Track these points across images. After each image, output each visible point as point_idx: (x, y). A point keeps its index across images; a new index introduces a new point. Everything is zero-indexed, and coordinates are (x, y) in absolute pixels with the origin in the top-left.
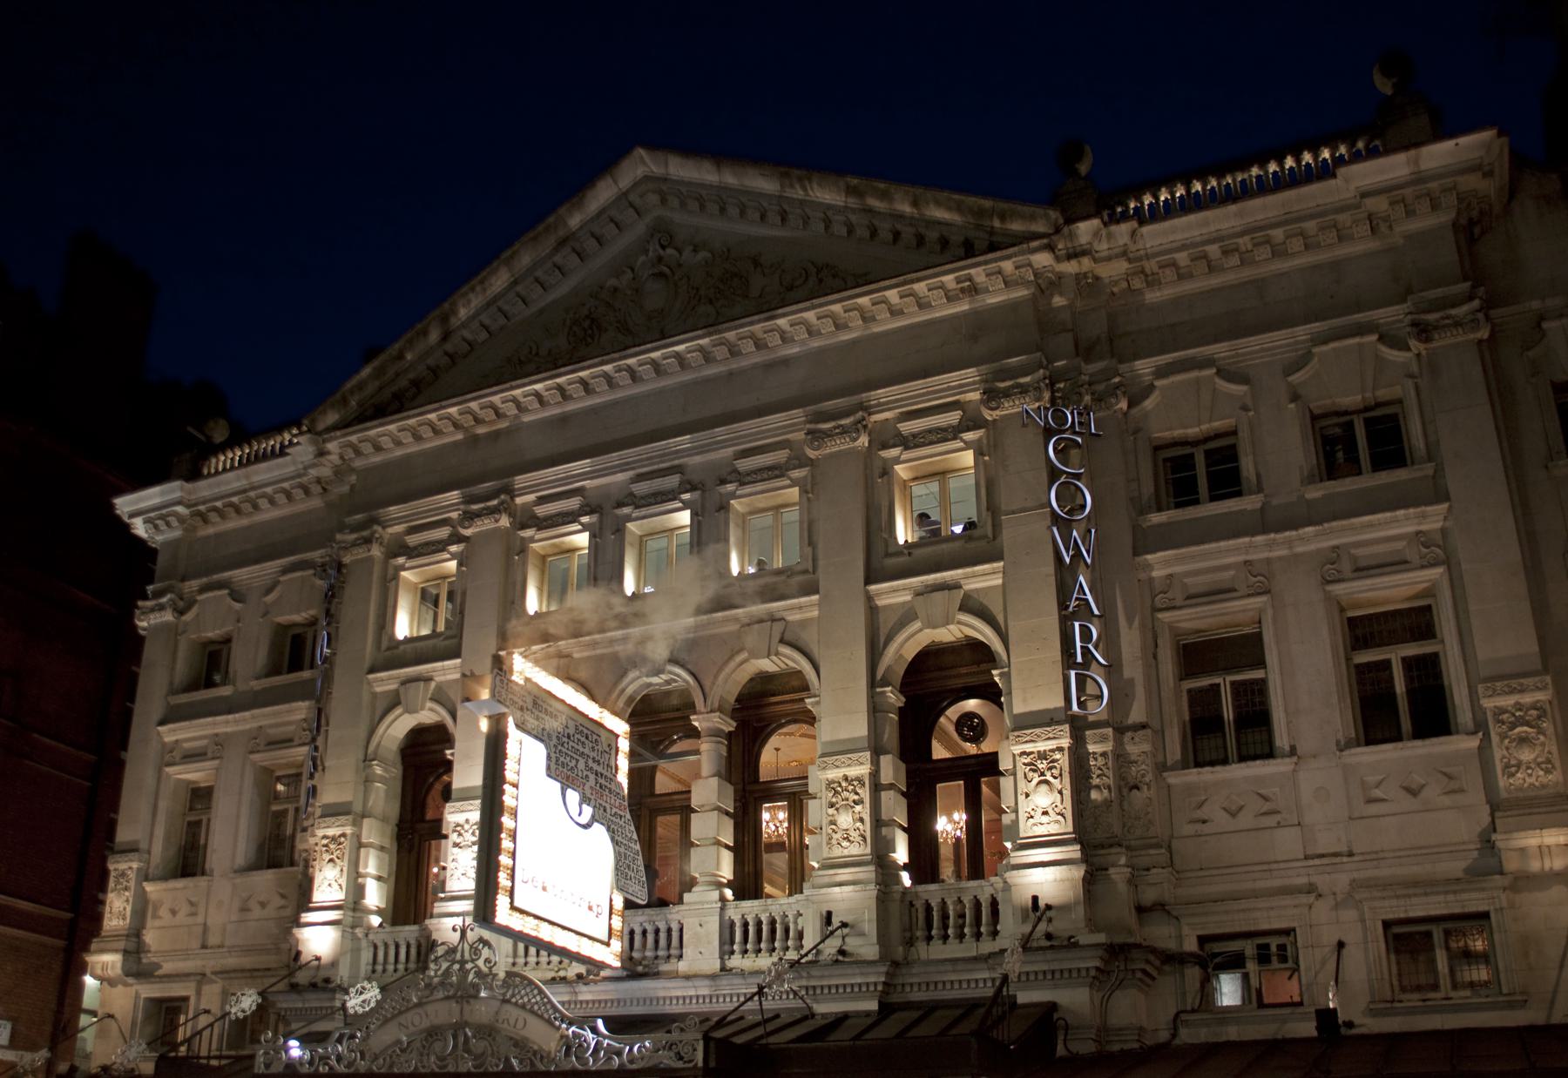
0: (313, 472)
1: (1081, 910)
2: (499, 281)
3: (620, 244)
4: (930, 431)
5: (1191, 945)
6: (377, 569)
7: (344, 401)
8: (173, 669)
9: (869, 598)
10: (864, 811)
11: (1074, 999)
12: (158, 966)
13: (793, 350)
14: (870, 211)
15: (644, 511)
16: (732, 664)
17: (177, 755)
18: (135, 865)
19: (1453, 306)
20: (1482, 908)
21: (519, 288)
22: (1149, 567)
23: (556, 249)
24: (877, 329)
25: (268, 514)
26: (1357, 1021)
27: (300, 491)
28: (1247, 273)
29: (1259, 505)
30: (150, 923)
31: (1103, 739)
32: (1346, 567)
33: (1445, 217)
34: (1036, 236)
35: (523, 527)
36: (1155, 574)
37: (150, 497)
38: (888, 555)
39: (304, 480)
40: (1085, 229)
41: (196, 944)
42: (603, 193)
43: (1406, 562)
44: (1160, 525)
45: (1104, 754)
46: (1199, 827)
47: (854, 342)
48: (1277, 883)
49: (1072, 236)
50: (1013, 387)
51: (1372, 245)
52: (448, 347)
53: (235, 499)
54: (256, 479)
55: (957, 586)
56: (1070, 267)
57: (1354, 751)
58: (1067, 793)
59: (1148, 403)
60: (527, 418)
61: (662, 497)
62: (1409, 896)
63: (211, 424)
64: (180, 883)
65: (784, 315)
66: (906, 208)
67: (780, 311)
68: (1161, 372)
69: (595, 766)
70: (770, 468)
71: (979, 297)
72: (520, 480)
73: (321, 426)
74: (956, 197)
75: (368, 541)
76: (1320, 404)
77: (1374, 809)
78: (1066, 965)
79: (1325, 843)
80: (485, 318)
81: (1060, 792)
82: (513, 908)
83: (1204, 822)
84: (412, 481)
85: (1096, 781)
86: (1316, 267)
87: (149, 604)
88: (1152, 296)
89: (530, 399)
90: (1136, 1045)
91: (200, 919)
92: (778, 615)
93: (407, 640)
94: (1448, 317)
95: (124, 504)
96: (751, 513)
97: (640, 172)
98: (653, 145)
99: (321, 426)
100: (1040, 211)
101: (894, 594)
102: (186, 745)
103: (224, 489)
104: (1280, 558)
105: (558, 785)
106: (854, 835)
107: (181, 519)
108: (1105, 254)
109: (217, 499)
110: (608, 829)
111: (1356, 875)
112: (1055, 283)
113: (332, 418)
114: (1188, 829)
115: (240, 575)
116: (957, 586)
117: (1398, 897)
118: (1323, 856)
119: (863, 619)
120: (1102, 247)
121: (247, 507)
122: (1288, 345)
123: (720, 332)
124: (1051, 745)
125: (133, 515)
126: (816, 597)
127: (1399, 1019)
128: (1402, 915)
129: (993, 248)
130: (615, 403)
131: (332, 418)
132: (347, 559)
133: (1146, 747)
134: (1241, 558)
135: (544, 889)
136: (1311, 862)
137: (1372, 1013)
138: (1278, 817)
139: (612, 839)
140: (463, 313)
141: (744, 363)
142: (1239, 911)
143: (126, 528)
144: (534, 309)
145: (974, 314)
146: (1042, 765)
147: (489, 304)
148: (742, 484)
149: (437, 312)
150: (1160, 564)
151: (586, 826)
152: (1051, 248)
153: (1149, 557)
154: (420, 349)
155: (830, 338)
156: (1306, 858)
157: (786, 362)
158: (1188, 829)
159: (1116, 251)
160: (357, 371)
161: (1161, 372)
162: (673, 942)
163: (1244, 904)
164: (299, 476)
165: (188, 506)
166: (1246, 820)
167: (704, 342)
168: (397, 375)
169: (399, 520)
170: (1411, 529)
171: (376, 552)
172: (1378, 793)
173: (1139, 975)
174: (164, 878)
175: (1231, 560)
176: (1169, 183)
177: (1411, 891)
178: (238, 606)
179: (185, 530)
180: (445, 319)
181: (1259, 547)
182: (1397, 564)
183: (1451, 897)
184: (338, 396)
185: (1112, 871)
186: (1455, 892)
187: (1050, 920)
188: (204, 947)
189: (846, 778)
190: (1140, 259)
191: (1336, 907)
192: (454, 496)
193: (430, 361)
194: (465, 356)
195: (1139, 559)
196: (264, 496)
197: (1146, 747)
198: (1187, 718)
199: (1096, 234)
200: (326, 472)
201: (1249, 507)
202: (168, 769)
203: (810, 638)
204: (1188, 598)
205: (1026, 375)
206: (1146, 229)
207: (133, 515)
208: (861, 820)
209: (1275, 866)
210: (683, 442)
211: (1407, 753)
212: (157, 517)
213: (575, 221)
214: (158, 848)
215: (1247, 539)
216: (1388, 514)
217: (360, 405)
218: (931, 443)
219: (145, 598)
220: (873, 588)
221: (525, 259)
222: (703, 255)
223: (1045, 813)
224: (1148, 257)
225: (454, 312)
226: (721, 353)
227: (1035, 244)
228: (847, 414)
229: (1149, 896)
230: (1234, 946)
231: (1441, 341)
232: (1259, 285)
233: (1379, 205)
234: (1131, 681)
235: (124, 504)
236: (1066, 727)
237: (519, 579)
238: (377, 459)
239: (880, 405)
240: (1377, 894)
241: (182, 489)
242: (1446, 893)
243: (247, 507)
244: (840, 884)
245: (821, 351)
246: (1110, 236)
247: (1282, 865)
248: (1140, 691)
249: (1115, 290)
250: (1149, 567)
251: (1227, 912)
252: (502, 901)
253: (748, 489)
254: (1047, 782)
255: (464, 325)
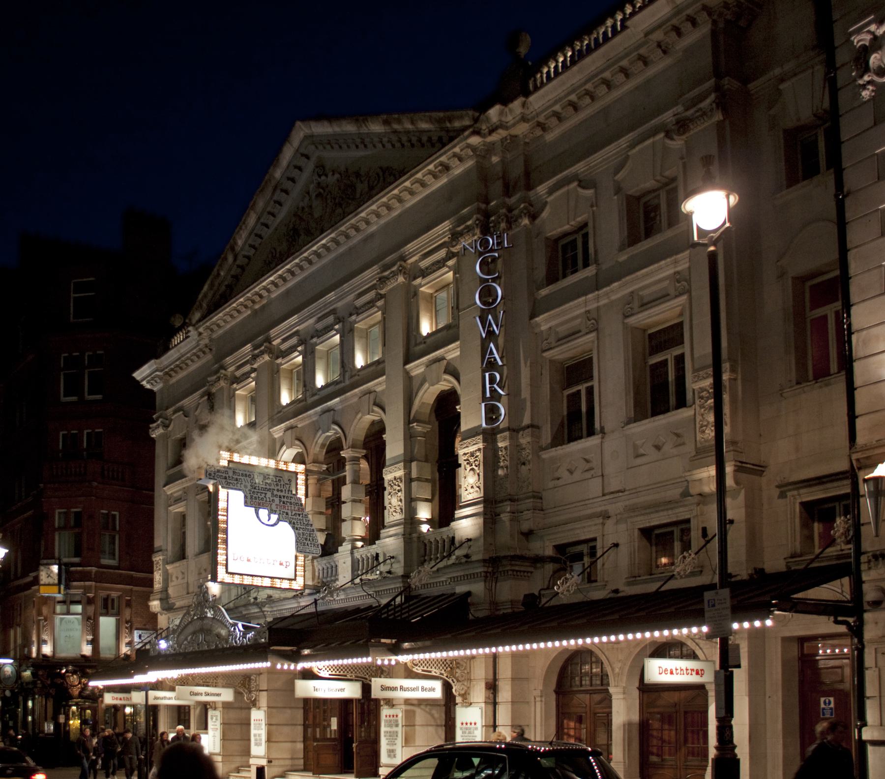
0: (202, 343)
1: (482, 540)
2: (252, 220)
3: (303, 178)
4: (433, 264)
5: (549, 552)
6: (226, 394)
7: (201, 306)
8: (167, 457)
9: (407, 373)
10: (401, 495)
11: (478, 588)
12: (174, 604)
13: (373, 228)
14: (395, 132)
15: (321, 339)
16: (356, 421)
17: (172, 500)
18: (161, 558)
19: (701, 102)
20: (687, 517)
21: (262, 220)
22: (538, 325)
23: (273, 194)
24: (408, 205)
25: (193, 367)
26: (621, 588)
27: (406, 193)
28: (598, 106)
29: (594, 272)
30: (171, 584)
31: (504, 439)
32: (636, 304)
33: (705, 29)
34: (465, 128)
35: (277, 358)
36: (543, 328)
37: (145, 371)
38: (416, 345)
39: (200, 347)
40: (494, 113)
41: (185, 592)
42: (287, 154)
43: (668, 295)
44: (546, 296)
45: (506, 448)
46: (556, 482)
47: (400, 216)
48: (589, 512)
49: (488, 119)
50: (464, 229)
51: (668, 61)
52: (238, 262)
53: (177, 363)
54: (182, 351)
55: (443, 358)
56: (494, 138)
57: (632, 425)
58: (482, 474)
59: (544, 215)
60: (273, 296)
61: (328, 329)
62: (649, 513)
63: (172, 319)
64: (177, 564)
65: (362, 211)
66: (409, 126)
67: (360, 209)
68: (551, 191)
69: (279, 493)
70: (368, 303)
71: (450, 172)
72: (273, 332)
73: (194, 321)
74: (427, 114)
75: (219, 379)
76: (633, 191)
77: (639, 461)
78: (471, 571)
79: (614, 484)
80: (250, 242)
81: (479, 475)
82: (227, 572)
83: (558, 479)
84: (223, 348)
85: (502, 464)
86: (637, 88)
87: (155, 425)
88: (550, 137)
89: (270, 286)
90: (510, 611)
91: (185, 581)
92: (372, 389)
93: (363, 368)
94: (697, 111)
95: (138, 375)
96: (370, 327)
97: (302, 135)
98: (303, 119)
99: (194, 321)
100: (464, 113)
101: (417, 368)
102: (175, 495)
103: (172, 359)
104: (604, 305)
105: (253, 509)
106: (398, 508)
107: (160, 378)
108: (512, 122)
109: (170, 365)
110: (290, 523)
111: (627, 503)
112: (490, 149)
113: (197, 316)
114: (551, 484)
115: (186, 402)
116: (443, 358)
117: (643, 515)
118: (612, 493)
119: (401, 386)
120: (509, 118)
121: (184, 366)
122: (618, 152)
123: (337, 229)
124: (475, 448)
125: (143, 380)
126: (458, 343)
127: (640, 586)
128: (675, 519)
129: (451, 139)
130: (306, 278)
131: (197, 316)
132: (214, 390)
133: (529, 439)
134: (583, 310)
135: (249, 560)
136: (607, 497)
137: (629, 584)
138: (592, 472)
139: (293, 528)
140: (240, 243)
141: (355, 241)
142: (569, 530)
143: (142, 386)
144: (272, 229)
145: (451, 183)
146: (472, 460)
147: (250, 234)
148: (358, 314)
149: (228, 247)
150: (544, 322)
151: (275, 524)
152: (477, 133)
153: (537, 319)
154: (224, 271)
155: (388, 217)
156: (604, 495)
157: (372, 236)
158: (551, 484)
159: (517, 118)
160: (202, 289)
161: (551, 191)
162: (333, 571)
163: (570, 526)
164: (198, 345)
165: (161, 371)
166: (577, 476)
167: (333, 235)
168: (219, 284)
169: (232, 364)
170: (671, 271)
171: (222, 383)
172: (641, 451)
173: (510, 573)
174: (172, 562)
175: (578, 312)
176: (561, 49)
177: (648, 511)
178: (187, 419)
179: (164, 382)
180: (233, 249)
181: (591, 302)
182: (663, 297)
183: (670, 512)
184: (197, 303)
185: (502, 516)
186: (672, 509)
187: (470, 547)
188: (188, 593)
189: (395, 479)
190: (533, 118)
191: (617, 523)
192: (249, 347)
193: (232, 273)
194: (247, 265)
195: (532, 321)
196: (188, 358)
197: (529, 439)
198: (565, 413)
199: (501, 113)
200: (207, 341)
201: (590, 274)
202: (170, 508)
203: (385, 401)
204: (559, 340)
205: (469, 219)
206: (532, 98)
207: (143, 380)
208: (401, 500)
209: (587, 502)
210: (331, 296)
211: (656, 424)
212: (152, 379)
213: (278, 174)
214: (170, 548)
215: (583, 298)
216: (656, 265)
217: (208, 305)
218: (434, 271)
219: (154, 422)
220: (407, 367)
221: (260, 204)
222: (337, 176)
223: (472, 487)
224: (538, 115)
225: (236, 243)
226: (342, 239)
227: (467, 133)
228: (393, 264)
229: (525, 526)
230: (579, 548)
231: (695, 129)
232: (605, 112)
233: (658, 36)
234: (525, 399)
235: (138, 375)
236: (481, 437)
237: (415, 314)
238: (221, 332)
239: (410, 254)
240: (632, 514)
241: (155, 363)
242: (667, 510)
243: (184, 366)
244: (391, 536)
245: (387, 224)
246: (511, 111)
247: (591, 501)
248: (528, 404)
249: (527, 140)
250: (538, 325)
251: (569, 530)
252: (221, 570)
253: (361, 317)
254: (472, 469)
255: (242, 249)
